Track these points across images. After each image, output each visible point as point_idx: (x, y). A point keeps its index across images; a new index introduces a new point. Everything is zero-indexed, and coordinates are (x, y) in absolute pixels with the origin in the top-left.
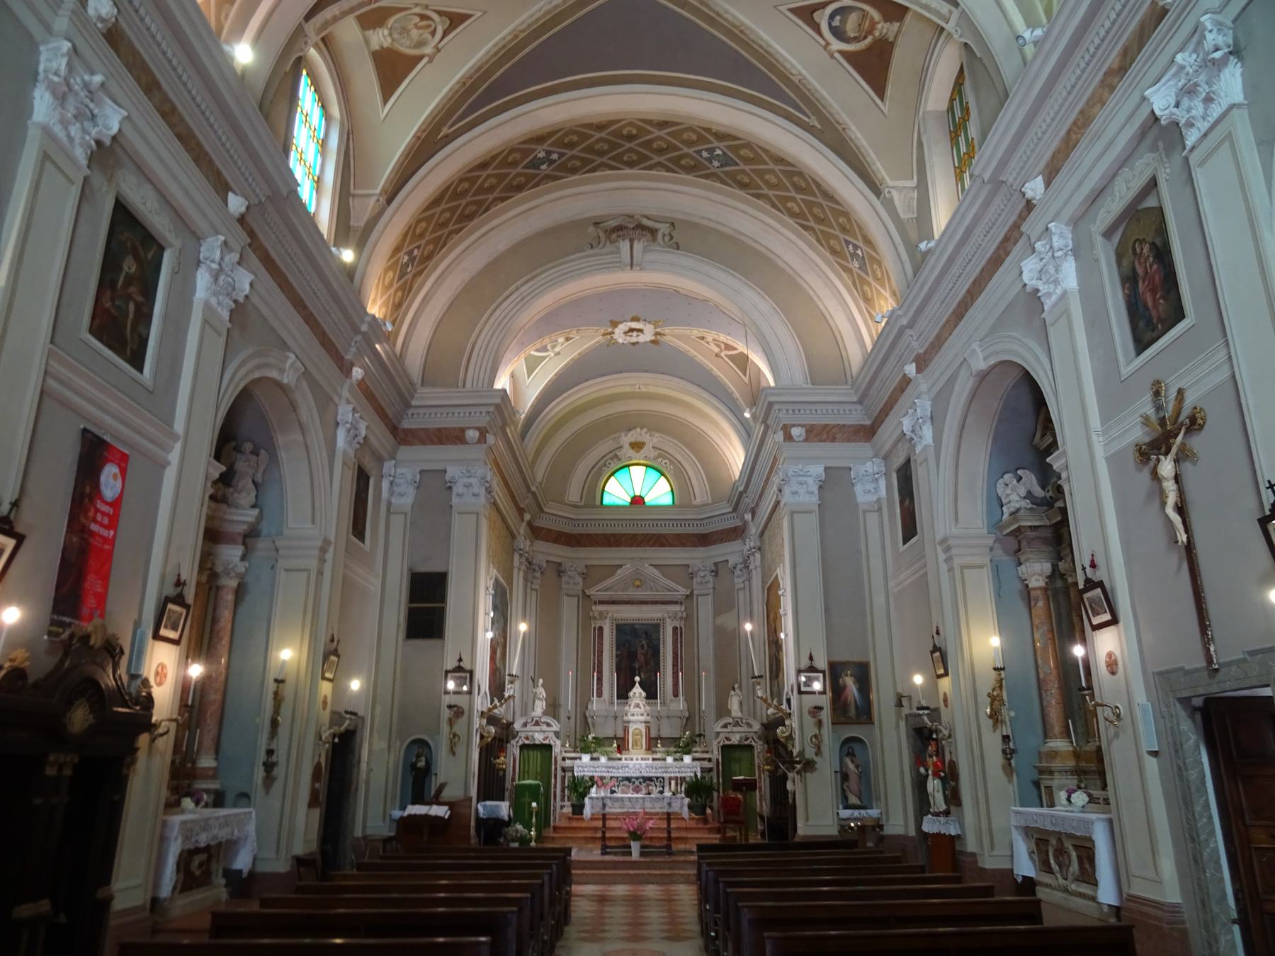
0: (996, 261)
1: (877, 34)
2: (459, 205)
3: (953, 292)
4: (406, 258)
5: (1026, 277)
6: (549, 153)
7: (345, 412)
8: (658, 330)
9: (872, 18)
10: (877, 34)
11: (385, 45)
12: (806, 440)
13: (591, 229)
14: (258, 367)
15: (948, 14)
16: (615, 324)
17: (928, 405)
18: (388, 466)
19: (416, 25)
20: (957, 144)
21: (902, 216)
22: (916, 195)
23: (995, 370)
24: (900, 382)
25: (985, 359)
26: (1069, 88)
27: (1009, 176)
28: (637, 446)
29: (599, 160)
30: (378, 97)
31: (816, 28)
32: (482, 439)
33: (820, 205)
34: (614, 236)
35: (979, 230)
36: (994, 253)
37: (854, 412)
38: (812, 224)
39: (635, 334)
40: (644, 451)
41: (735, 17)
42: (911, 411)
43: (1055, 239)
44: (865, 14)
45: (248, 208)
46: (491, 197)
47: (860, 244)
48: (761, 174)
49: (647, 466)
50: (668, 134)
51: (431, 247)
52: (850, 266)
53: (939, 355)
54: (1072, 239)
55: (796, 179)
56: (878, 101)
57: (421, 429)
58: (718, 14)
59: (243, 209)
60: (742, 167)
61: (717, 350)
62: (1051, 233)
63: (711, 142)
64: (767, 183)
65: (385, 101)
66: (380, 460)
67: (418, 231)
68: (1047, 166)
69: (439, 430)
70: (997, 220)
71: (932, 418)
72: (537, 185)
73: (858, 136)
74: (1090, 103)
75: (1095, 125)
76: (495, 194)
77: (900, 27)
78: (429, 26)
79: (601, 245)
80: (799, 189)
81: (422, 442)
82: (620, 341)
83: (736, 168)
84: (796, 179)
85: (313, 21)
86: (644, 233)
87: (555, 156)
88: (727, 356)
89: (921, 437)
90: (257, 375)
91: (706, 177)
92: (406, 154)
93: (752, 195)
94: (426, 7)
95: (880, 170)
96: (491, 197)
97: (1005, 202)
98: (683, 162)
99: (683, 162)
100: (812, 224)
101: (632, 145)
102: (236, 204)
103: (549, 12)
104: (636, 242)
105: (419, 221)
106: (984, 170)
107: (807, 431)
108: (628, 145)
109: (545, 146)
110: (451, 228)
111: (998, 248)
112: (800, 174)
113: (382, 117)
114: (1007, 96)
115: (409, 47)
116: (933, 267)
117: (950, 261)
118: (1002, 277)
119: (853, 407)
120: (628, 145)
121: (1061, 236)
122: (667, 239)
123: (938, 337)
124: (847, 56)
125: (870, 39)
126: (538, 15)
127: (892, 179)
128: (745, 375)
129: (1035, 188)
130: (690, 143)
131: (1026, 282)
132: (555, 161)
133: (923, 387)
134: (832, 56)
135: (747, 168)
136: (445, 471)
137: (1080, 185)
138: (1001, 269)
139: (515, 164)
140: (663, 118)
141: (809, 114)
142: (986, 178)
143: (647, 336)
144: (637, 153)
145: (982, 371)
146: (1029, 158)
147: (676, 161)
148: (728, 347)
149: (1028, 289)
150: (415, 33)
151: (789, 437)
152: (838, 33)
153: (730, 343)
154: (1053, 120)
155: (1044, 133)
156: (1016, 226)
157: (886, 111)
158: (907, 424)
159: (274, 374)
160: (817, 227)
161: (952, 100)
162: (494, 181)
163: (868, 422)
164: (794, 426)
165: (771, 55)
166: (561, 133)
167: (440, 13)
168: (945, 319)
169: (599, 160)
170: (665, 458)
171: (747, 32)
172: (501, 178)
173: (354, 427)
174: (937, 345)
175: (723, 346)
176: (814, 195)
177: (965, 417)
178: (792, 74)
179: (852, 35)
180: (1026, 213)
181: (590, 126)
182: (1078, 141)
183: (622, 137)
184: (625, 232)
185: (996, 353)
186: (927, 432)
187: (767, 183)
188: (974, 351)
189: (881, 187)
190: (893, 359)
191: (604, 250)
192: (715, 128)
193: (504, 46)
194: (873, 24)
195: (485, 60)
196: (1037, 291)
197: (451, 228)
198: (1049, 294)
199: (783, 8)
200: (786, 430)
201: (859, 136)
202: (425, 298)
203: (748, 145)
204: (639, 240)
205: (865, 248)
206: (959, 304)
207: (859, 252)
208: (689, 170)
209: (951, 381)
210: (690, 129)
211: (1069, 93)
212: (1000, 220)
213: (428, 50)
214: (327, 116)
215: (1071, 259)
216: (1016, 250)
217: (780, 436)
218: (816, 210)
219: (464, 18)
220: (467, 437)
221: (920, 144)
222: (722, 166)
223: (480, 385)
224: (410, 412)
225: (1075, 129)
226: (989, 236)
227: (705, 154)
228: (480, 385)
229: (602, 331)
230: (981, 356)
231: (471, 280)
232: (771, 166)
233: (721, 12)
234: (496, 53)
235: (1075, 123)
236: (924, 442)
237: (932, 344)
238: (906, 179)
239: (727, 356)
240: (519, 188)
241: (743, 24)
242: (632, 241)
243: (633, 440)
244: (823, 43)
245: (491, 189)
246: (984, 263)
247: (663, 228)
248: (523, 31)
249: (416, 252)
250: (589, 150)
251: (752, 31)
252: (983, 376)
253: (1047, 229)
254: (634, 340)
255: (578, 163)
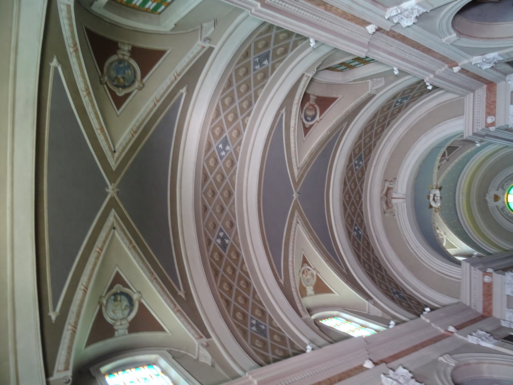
0: (403, 39)
1: (314, 103)
2: (375, 269)
3: (418, 56)
4: (397, 295)
5: (410, 24)
6: (355, 230)
7: (472, 340)
8: (434, 187)
9: (309, 106)
10: (314, 103)
11: (312, 288)
12: (494, 115)
13: (387, 215)
14: (445, 376)
15: (307, 77)
16: (431, 207)
17: (475, 58)
18: (504, 324)
19: (306, 276)
20: (354, 66)
21: (384, 84)
22: (375, 80)
23: (457, 28)
24: (463, 73)
25: (450, 34)
26: (331, 24)
27: (366, 40)
28: (496, 198)
29: (358, 210)
30: (331, 295)
31: (311, 126)
32: (490, 274)
33: (379, 119)
34: (390, 205)
35: (389, 49)
36: (400, 41)
37: (479, 94)
38: (387, 122)
39: (436, 198)
40: (500, 195)
41: (307, 157)
42: (479, 66)
43: (392, 15)
44: (307, 108)
45: (370, 360)
46: (372, 255)
47: (395, 100)
48: (365, 144)
49: (508, 194)
50: (349, 182)
51: (392, 284)
52: (406, 103)
53: (448, 57)
54: (393, 7)
55: (368, 130)
56: (338, 100)
57: (483, 303)
58: (306, 163)
59: (371, 362)
60: (362, 152)
61: (445, 161)
62: (390, 17)
63: (352, 165)
64: (369, 142)
65: (332, 292)
66: (501, 328)
67: (385, 288)
68: (362, 26)
69: (484, 295)
70: (385, 42)
71: (483, 55)
72: (367, 236)
73: (351, 105)
74: (337, 14)
75: (346, 10)
76: (371, 254)
77: (312, 95)
78: (306, 271)
79: (394, 211)
80: (372, 128)
81: (490, 304)
82: (439, 205)
83: (363, 155)
84: (368, 130)
85: (302, 314)
86: (389, 192)
87: (356, 228)
88: (448, 155)
89: (494, 58)
90: (450, 378)
91: (366, 167)
92: (353, 288)
93: (374, 148)
94: (300, 271)
95: (364, 96)
96: (372, 255)
97: (377, 40)
98: (360, 176)
99: (360, 176)
100: (387, 122)
101: (353, 196)
102: (368, 364)
103: (303, 226)
104: (393, 196)
105: (381, 287)
106: (363, 52)
107: (490, 115)
108: (353, 199)
109: (352, 231)
110: (384, 274)
111: (397, 39)
112: (366, 129)
113: (338, 295)
114: (336, 48)
115: (313, 280)
116: (407, 67)
117: (403, 59)
118: (410, 35)
119: (476, 94)
120: (353, 199)
121: (392, 12)
122: (392, 183)
123: (439, 59)
124: (321, 114)
125: (316, 106)
126: (304, 230)
127: (368, 90)
128: (458, 147)
129: (371, 29)
130: (353, 174)
131: (412, 23)
132: (358, 228)
133: (466, 61)
134: (321, 119)
135: (363, 150)
136: (508, 296)
137: (370, 10)
138: (407, 36)
139: (359, 244)
140: (343, 184)
141: (342, 126)
142: (366, 50)
143: (438, 192)
144: (356, 195)
145: (457, 35)
146: (359, 34)
147: (359, 179)
148: (444, 155)
149: (416, 21)
150: (309, 277)
151: (493, 124)
152: (313, 118)
153: (441, 155)
154: (343, 27)
155: (349, 30)
156: (388, 33)
157: (342, 96)
158: (488, 66)
159: (449, 370)
160: (388, 120)
161: (338, 71)
162: (365, 254)
163: (485, 86)
164: (486, 122)
165: (320, 143)
166: (378, 261)
167: (302, 266)
168: (432, 58)
169: (358, 210)
170: (504, 185)
171: (312, 152)
172: (364, 250)
173: (480, 337)
174: (444, 59)
175: (443, 158)
176: (374, 122)
177: (482, 38)
178: (327, 134)
179: (314, 112)
180: (382, 31)
181: (345, 213)
182: (352, 15)
183: (349, 201)
184: (388, 201)
185: (448, 30)
186: (491, 56)
187: (369, 142)
188: (447, 41)
189: (372, 94)
190: (451, 78)
191: (396, 210)
192: (347, 164)
193: (315, 244)
194: (310, 105)
195: (319, 252)
196: (417, 17)
197: (384, 274)
198: (418, 11)
199: (304, 139)
200: (488, 126)
201: (351, 106)
202: (415, 290)
203: (354, 150)
204: (392, 195)
205: (398, 98)
206: (423, 52)
207: (399, 100)
208: (363, 174)
209: (462, 48)
210: (347, 173)
211: (333, 23)
212: (385, 41)
213: (315, 273)
214: (338, 316)
215: (402, 5)
216: (397, 30)
217: (492, 129)
218: (381, 121)
219: (304, 258)
220: (488, 282)
221: (354, 81)
222: (362, 161)
223: (460, 272)
224: (473, 307)
225: (347, 18)
226: (392, 44)
227: (357, 167)
228: (460, 272)
229: (434, 212)
230: (449, 37)
231: (408, 268)
232: (362, 140)
233: (305, 162)
234: (317, 247)
235: (345, 18)
236: (497, 57)
237: (443, 61)
238: (368, 85)
239: (448, 155)
240: (369, 243)
241: (309, 154)
242: (392, 198)
243: (493, 200)
244: (316, 123)
245: (368, 255)
246: (404, 45)
247: (387, 184)
248: (309, 236)
249: (394, 291)
250: (354, 214)
251: (312, 150)
252: (460, 34)
253: (388, 19)
254: (439, 198)
255: (359, 219)
